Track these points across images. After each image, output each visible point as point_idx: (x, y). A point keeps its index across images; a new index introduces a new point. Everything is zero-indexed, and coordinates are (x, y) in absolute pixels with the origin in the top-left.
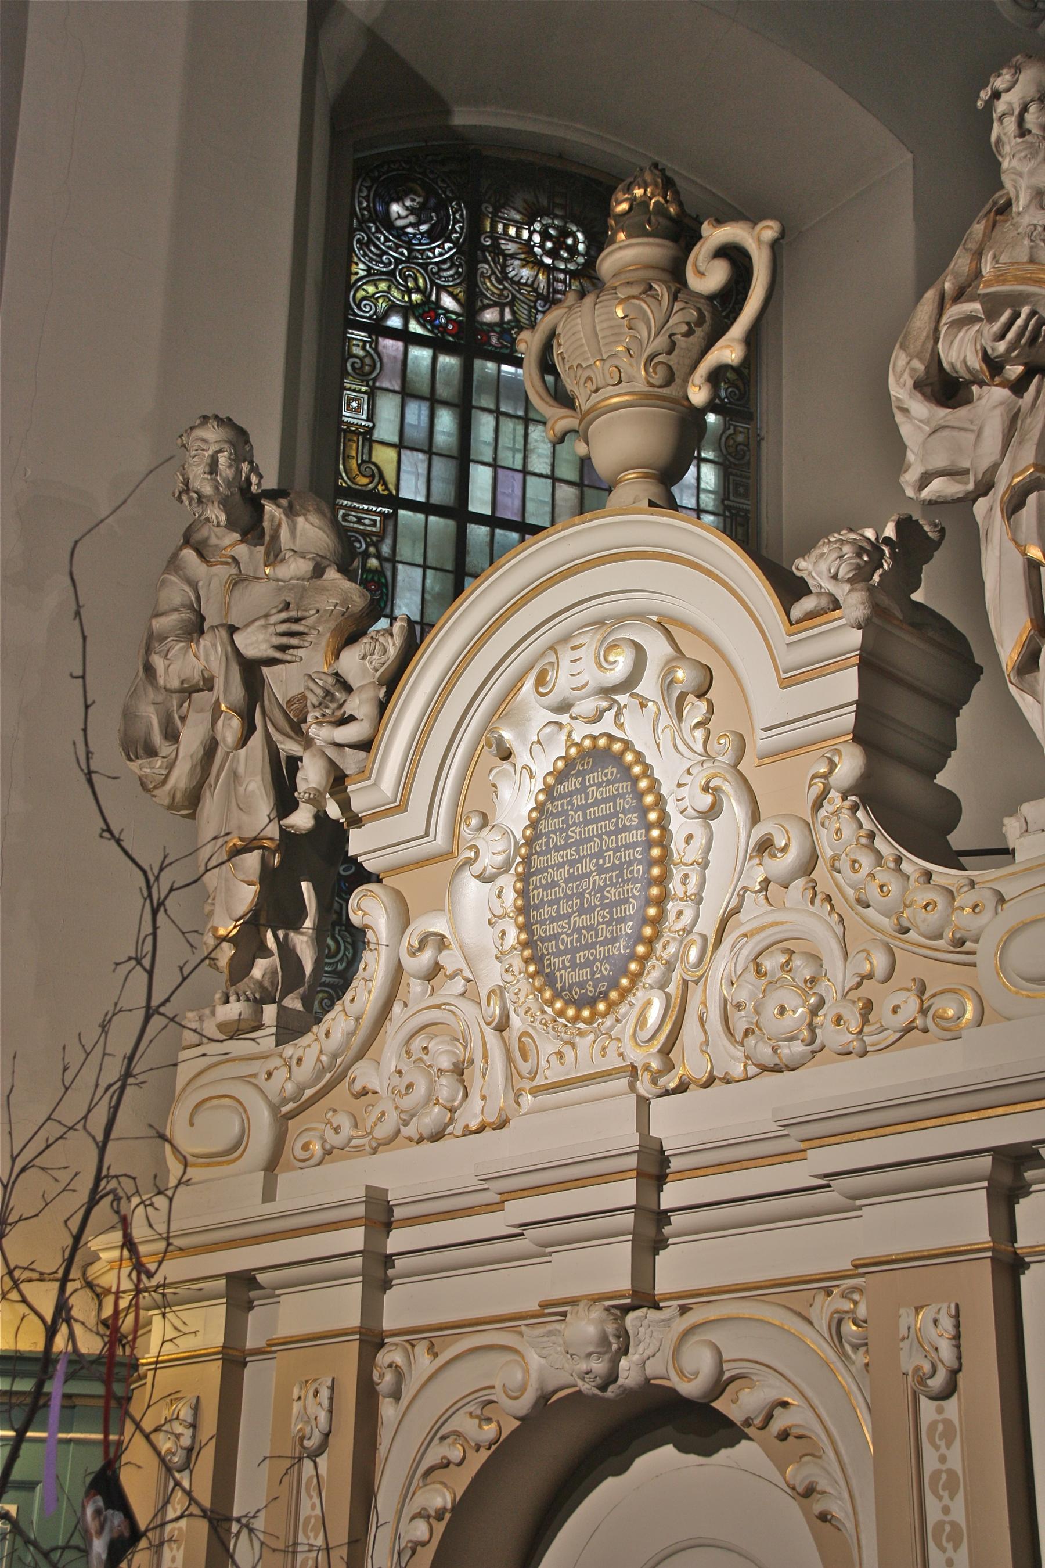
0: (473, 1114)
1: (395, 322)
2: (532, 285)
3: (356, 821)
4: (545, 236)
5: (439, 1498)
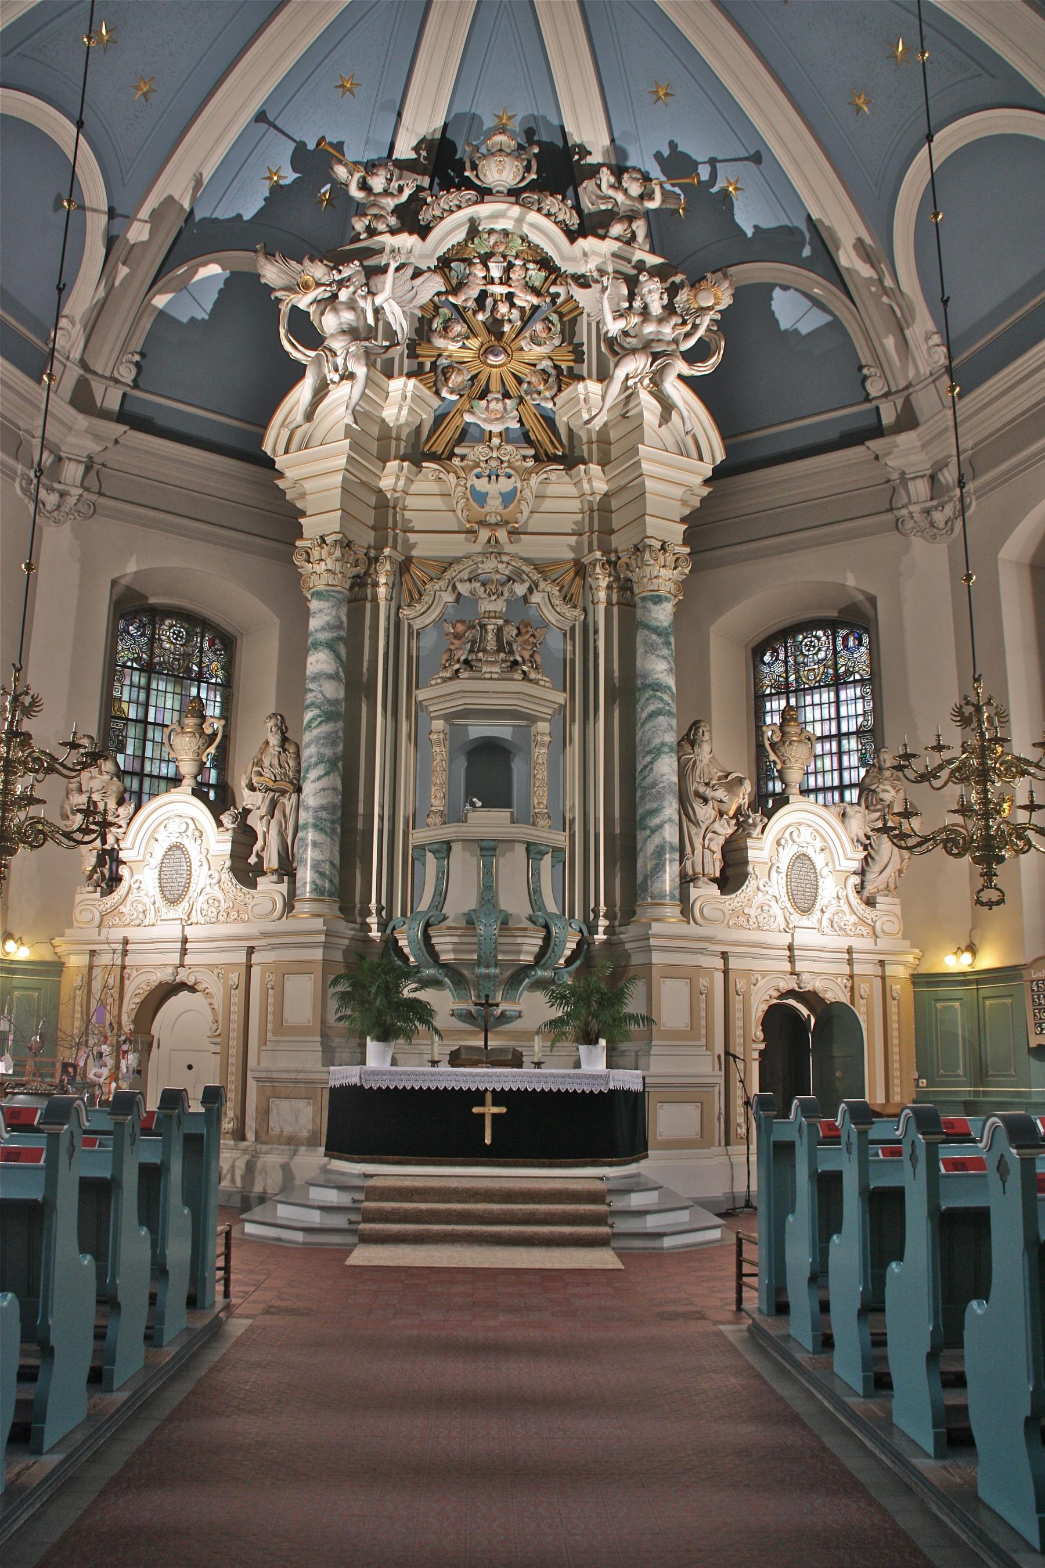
0: (146, 922)
1: (129, 664)
2: (169, 650)
4: (174, 633)
5: (138, 1000)
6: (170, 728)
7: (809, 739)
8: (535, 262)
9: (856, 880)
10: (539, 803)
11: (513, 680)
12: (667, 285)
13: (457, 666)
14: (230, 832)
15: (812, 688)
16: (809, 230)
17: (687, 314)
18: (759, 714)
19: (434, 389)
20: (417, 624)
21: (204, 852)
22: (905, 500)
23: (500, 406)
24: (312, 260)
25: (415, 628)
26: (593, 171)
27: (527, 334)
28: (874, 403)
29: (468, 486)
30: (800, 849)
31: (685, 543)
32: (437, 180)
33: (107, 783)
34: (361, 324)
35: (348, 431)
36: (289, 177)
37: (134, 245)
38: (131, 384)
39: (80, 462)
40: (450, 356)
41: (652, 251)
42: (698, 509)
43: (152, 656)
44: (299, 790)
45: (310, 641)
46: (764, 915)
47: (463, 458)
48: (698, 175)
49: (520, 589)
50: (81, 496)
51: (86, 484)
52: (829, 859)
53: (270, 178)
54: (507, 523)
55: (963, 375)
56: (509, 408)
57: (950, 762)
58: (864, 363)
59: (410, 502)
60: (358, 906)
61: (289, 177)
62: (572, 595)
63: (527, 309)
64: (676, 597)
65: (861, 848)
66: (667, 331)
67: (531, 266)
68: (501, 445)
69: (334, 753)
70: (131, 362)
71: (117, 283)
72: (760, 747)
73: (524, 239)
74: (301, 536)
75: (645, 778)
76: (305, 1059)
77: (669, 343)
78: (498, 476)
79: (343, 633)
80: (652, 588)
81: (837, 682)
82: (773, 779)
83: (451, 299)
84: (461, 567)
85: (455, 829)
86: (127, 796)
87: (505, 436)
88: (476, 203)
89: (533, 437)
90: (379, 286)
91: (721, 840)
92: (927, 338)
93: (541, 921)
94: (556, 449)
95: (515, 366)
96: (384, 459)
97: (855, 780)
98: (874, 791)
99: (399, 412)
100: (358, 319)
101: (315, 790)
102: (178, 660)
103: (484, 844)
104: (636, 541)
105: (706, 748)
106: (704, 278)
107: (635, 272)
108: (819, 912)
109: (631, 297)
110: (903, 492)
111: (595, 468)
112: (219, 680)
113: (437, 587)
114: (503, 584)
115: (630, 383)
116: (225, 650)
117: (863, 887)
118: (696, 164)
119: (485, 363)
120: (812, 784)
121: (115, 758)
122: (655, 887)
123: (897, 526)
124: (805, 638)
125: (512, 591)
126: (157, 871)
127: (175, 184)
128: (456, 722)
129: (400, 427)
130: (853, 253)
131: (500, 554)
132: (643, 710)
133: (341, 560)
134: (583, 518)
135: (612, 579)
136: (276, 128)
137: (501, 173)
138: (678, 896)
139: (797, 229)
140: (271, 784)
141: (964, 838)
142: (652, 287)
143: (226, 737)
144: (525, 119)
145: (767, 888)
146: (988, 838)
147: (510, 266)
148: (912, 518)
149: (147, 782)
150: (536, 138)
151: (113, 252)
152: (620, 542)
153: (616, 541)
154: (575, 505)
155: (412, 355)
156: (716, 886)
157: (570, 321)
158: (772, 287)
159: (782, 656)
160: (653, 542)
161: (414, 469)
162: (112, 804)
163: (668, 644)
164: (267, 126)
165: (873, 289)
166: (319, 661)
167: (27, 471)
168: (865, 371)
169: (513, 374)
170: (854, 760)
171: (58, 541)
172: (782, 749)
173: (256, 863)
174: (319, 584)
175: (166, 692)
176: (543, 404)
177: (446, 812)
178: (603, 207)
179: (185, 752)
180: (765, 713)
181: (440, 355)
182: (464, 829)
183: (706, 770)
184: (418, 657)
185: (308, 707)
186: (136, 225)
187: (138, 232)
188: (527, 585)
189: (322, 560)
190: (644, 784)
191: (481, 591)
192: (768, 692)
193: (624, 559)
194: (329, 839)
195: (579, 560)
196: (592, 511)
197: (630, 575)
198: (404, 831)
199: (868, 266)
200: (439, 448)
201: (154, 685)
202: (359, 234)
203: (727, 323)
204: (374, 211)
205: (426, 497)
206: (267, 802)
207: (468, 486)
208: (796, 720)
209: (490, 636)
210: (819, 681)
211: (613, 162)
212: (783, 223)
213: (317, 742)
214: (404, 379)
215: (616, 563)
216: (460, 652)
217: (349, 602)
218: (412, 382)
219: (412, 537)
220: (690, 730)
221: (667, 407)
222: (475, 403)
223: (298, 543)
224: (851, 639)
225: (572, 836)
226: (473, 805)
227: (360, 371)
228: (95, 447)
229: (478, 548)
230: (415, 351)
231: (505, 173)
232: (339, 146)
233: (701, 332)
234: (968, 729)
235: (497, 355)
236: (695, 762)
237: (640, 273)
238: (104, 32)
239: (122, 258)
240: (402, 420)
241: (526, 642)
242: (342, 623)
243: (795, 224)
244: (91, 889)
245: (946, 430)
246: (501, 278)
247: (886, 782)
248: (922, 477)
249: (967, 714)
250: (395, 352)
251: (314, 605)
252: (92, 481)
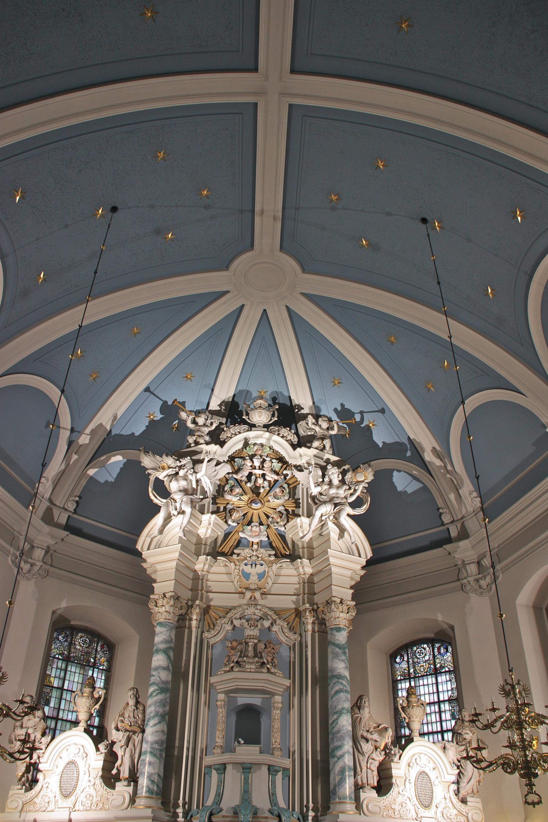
0: (49, 809)
1: (57, 656)
2: (79, 650)
3: (40, 763)
4: (83, 641)
6: (76, 693)
7: (422, 704)
8: (276, 459)
9: (454, 787)
10: (275, 742)
11: (262, 672)
12: (341, 470)
13: (232, 665)
14: (103, 755)
15: (423, 676)
16: (409, 444)
17: (351, 484)
18: (395, 690)
19: (225, 520)
20: (212, 641)
21: (87, 766)
22: (465, 575)
23: (258, 529)
24: (167, 456)
25: (211, 643)
26: (304, 417)
27: (272, 493)
28: (446, 526)
29: (241, 569)
30: (422, 768)
31: (353, 599)
32: (229, 420)
33: (38, 723)
34: (189, 487)
35: (181, 540)
36: (158, 416)
37: (81, 445)
38: (73, 511)
39: (43, 549)
40: (233, 504)
41: (334, 454)
42: (359, 582)
43: (69, 652)
44: (143, 731)
45: (154, 649)
46: (403, 809)
47: (238, 555)
48: (355, 419)
49: (267, 624)
50: (41, 566)
51: (45, 560)
52: (438, 775)
53: (149, 417)
54: (260, 589)
55: (489, 511)
56: (262, 530)
57: (501, 717)
58: (440, 507)
59: (211, 577)
60: (172, 801)
61: (158, 416)
62: (294, 627)
63: (272, 481)
64: (348, 628)
65: (456, 768)
66: (342, 492)
67: (274, 461)
68: (258, 549)
69: (164, 711)
70: (74, 501)
71: (71, 463)
72: (396, 709)
74: (153, 593)
75: (333, 727)
77: (342, 498)
78: (256, 565)
79: (172, 645)
80: (336, 623)
81: (436, 672)
82: (404, 727)
83: (234, 476)
84: (236, 611)
85: (228, 756)
86: (47, 731)
87: (260, 544)
88: (248, 431)
89: (274, 545)
90: (199, 469)
91: (377, 764)
92: (470, 494)
93: (276, 812)
94: (286, 551)
95: (266, 509)
96: (198, 554)
97: (449, 728)
98: (460, 734)
99: (207, 531)
100: (188, 484)
101: (153, 732)
102: (84, 655)
103: (244, 765)
104: (327, 599)
105: (367, 710)
106: (359, 466)
107: (325, 464)
108: (435, 807)
109: (323, 476)
110: (464, 570)
111: (306, 561)
112: (104, 668)
113: (223, 622)
114: (258, 621)
115: (323, 518)
116: (109, 651)
117: (458, 792)
118: (353, 414)
119: (250, 508)
120: (426, 730)
121: (44, 709)
122: (340, 792)
123: (462, 588)
124: (417, 648)
125: (262, 625)
126: (59, 777)
127: (104, 418)
128: (231, 695)
129: (207, 539)
130: (431, 454)
131: (256, 605)
132: (332, 689)
133: (173, 606)
134: (300, 587)
135: (315, 618)
136: (154, 394)
137: (260, 417)
138: (353, 797)
139: (403, 443)
140: (128, 728)
141: (513, 763)
142: (333, 471)
143: (105, 699)
144: (272, 392)
145: (404, 793)
146: (526, 762)
147: (264, 461)
148: (470, 584)
149: (60, 723)
150: (277, 401)
151: (72, 446)
152: (319, 599)
153: (316, 598)
154: (296, 580)
155: (214, 503)
156: (375, 791)
157: (293, 487)
158: (393, 470)
159: (406, 659)
160: (336, 599)
161: (213, 560)
162: (39, 735)
163: (345, 653)
164: (149, 394)
165: (442, 471)
166: (159, 660)
167: (15, 552)
168: (441, 511)
169: (265, 513)
170: (448, 716)
171: (27, 589)
172: (408, 710)
173: (116, 774)
174: (161, 618)
175: (75, 673)
176: (279, 528)
177: (224, 746)
178: (309, 433)
179: (82, 708)
180: (398, 690)
181: (228, 503)
182: (233, 756)
183: (367, 723)
184: (212, 659)
185: (151, 685)
186: (83, 436)
187: (84, 439)
188: (270, 621)
189: (163, 606)
190: (333, 731)
192: (399, 678)
193: (321, 608)
194: (158, 761)
195: (298, 608)
196: (304, 583)
197: (324, 616)
198: (200, 757)
199: (439, 460)
200: (226, 550)
201: (69, 669)
202: (191, 444)
203: (371, 488)
204: (199, 433)
206: (125, 737)
207: (241, 569)
208: (415, 694)
209: (250, 649)
210: (426, 672)
211: (314, 413)
212: (396, 441)
213: (155, 704)
214: (210, 515)
215: (317, 610)
216: (234, 657)
217: (177, 628)
218: (214, 516)
219: (211, 595)
220: (358, 701)
221: (342, 530)
222: (245, 527)
223: (152, 596)
224: (442, 648)
225: (294, 761)
226: (239, 742)
227: (188, 510)
228: (51, 542)
229: (245, 601)
230: (216, 501)
231: (262, 417)
232: (183, 404)
233: (358, 493)
234: (509, 698)
235: (256, 504)
236: (361, 719)
237: (327, 465)
238: (79, 352)
239: (75, 451)
240: (208, 535)
241: (269, 652)
242: (172, 639)
243: (403, 441)
244: (20, 787)
245: (483, 539)
246: (259, 467)
247: (467, 728)
248: (473, 563)
249: (507, 690)
250: (206, 501)
251: (158, 629)
252: (48, 559)
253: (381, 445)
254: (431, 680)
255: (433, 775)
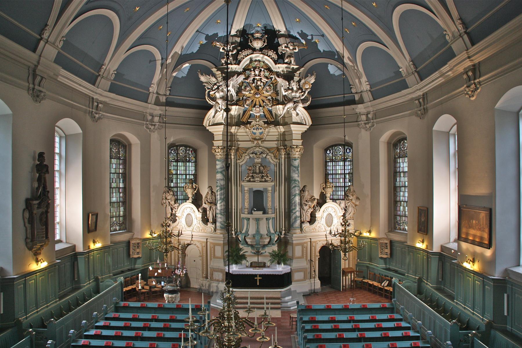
9: (342, 218)
18: (326, 166)
20: (241, 164)
36: (204, 42)
43: (177, 158)
49: (264, 156)
61: (204, 42)
66: (298, 95)
73: (264, 62)
76: (220, 264)
77: (298, 98)
94: (273, 121)
101: (220, 206)
105: (307, 192)
118: (308, 36)
127: (177, 49)
129: (235, 115)
147: (261, 71)
166: (219, 176)
187: (169, 61)
191: (255, 156)
205: (240, 132)
209: (257, 169)
251: (217, 162)
253: (322, 51)
254: (341, 163)
255: (333, 214)
